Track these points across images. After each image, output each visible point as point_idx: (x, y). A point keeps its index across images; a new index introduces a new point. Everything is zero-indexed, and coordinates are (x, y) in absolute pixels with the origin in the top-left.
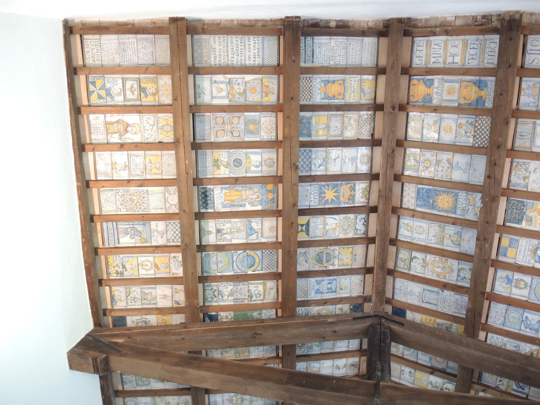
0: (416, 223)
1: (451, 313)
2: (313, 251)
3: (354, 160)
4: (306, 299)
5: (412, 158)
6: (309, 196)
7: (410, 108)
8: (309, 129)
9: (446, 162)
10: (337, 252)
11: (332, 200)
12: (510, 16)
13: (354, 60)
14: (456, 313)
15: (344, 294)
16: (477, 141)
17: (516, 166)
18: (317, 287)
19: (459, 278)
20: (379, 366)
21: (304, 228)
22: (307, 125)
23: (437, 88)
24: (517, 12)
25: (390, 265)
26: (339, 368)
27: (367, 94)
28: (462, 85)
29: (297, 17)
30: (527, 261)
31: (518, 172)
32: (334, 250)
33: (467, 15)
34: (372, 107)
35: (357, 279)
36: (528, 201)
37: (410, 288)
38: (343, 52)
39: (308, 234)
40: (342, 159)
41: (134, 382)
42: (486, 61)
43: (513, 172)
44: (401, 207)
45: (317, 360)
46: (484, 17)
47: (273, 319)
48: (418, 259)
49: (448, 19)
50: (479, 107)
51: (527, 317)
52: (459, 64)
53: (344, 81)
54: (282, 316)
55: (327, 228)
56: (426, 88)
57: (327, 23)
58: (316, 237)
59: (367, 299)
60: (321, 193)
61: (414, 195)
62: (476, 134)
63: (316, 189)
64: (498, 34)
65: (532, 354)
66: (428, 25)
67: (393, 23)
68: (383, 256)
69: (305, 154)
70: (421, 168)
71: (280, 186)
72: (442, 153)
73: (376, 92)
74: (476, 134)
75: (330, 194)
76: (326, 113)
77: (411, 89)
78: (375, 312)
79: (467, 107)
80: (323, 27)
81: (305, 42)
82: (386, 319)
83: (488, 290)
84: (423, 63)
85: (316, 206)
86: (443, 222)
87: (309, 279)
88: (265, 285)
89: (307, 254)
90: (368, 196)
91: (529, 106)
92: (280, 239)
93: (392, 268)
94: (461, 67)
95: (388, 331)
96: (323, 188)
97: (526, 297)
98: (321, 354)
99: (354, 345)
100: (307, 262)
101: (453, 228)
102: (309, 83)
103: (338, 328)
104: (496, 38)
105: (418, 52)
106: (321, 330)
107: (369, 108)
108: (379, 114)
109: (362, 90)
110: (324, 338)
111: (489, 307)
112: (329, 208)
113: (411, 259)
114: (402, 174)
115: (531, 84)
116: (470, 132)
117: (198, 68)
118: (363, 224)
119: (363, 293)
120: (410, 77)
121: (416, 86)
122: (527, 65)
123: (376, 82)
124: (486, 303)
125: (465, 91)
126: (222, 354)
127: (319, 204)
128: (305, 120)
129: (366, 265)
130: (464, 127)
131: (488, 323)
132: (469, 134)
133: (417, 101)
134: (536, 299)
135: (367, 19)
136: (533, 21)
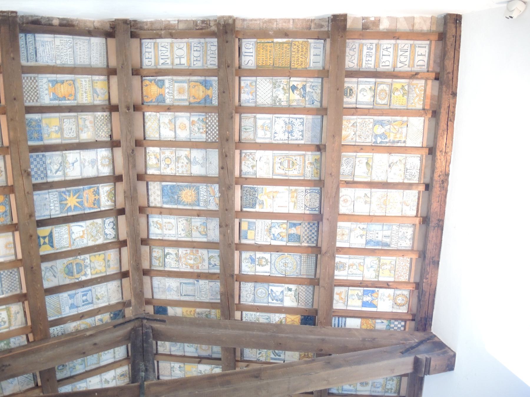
0: (165, 220)
1: (208, 301)
2: (60, 264)
3: (94, 162)
4: (60, 317)
5: (153, 157)
6: (48, 204)
7: (145, 109)
8: (40, 132)
9: (185, 158)
10: (88, 261)
11: (75, 206)
12: (225, 21)
13: (82, 60)
14: (212, 299)
15: (102, 304)
16: (209, 136)
17: (244, 156)
18: (70, 302)
19: (210, 266)
20: (142, 366)
21: (47, 240)
22: (37, 128)
23: (168, 88)
24: (230, 17)
25: (146, 265)
27: (100, 94)
28: (190, 84)
29: (13, 12)
30: (265, 240)
31: (247, 162)
32: (84, 260)
33: (188, 19)
34: (107, 108)
35: (113, 285)
36: (258, 186)
37: (167, 285)
38: (69, 52)
39: (52, 246)
40: (81, 163)
42: (209, 63)
43: (243, 162)
44: (149, 206)
45: (82, 379)
46: (203, 22)
47: (24, 346)
48: (171, 254)
49: (171, 22)
50: (207, 105)
51: (272, 290)
52: (186, 65)
53: (74, 81)
54: (34, 341)
55: (74, 236)
56: (159, 89)
57: (49, 20)
58: (61, 248)
59: (126, 304)
60: (62, 201)
61: (159, 193)
62: (207, 130)
63: (56, 196)
64: (216, 37)
65: (281, 322)
66: (154, 27)
67: (119, 24)
68: (136, 257)
69: (38, 159)
70: (163, 166)
71: (12, 196)
72: (180, 150)
73: (109, 93)
74: (207, 130)
75: (72, 201)
76: (57, 115)
77: (144, 90)
78: (136, 315)
79: (197, 105)
80: (45, 25)
81: (26, 39)
82: (148, 319)
83: (236, 272)
84: (153, 65)
85: (58, 214)
86: (189, 216)
87: (61, 295)
88: (8, 310)
89: (54, 267)
90: (114, 199)
91: (249, 102)
92: (20, 256)
93: (148, 268)
94: (187, 68)
95: (150, 331)
96: (63, 194)
97: (269, 272)
98: (87, 372)
100: (55, 277)
101: (200, 220)
102: (35, 83)
103: (97, 340)
104: (215, 41)
105: (147, 53)
106: (80, 345)
107: (103, 109)
108: (115, 114)
109: (94, 91)
110: (84, 353)
111: (240, 287)
112: (73, 216)
113: (165, 256)
114: (146, 173)
115: (249, 82)
116: (203, 129)
118: (113, 228)
119: (123, 298)
120: (142, 78)
121: (149, 86)
122: (243, 66)
123: (109, 83)
124: (237, 284)
125: (193, 91)
127: (61, 212)
128: (34, 123)
129: (121, 269)
130: (196, 125)
131: (241, 303)
132: (201, 130)
133: (151, 101)
134: (276, 273)
135: (92, 19)
136: (245, 26)
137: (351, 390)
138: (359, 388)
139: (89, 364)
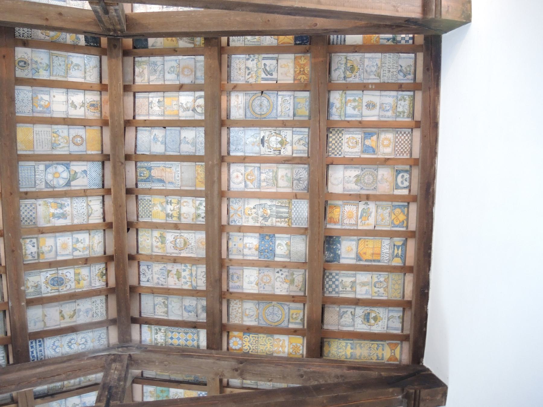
26: (75, 107)
99: (92, 77)
137: (356, 116)
138: (365, 112)
139: (54, 74)
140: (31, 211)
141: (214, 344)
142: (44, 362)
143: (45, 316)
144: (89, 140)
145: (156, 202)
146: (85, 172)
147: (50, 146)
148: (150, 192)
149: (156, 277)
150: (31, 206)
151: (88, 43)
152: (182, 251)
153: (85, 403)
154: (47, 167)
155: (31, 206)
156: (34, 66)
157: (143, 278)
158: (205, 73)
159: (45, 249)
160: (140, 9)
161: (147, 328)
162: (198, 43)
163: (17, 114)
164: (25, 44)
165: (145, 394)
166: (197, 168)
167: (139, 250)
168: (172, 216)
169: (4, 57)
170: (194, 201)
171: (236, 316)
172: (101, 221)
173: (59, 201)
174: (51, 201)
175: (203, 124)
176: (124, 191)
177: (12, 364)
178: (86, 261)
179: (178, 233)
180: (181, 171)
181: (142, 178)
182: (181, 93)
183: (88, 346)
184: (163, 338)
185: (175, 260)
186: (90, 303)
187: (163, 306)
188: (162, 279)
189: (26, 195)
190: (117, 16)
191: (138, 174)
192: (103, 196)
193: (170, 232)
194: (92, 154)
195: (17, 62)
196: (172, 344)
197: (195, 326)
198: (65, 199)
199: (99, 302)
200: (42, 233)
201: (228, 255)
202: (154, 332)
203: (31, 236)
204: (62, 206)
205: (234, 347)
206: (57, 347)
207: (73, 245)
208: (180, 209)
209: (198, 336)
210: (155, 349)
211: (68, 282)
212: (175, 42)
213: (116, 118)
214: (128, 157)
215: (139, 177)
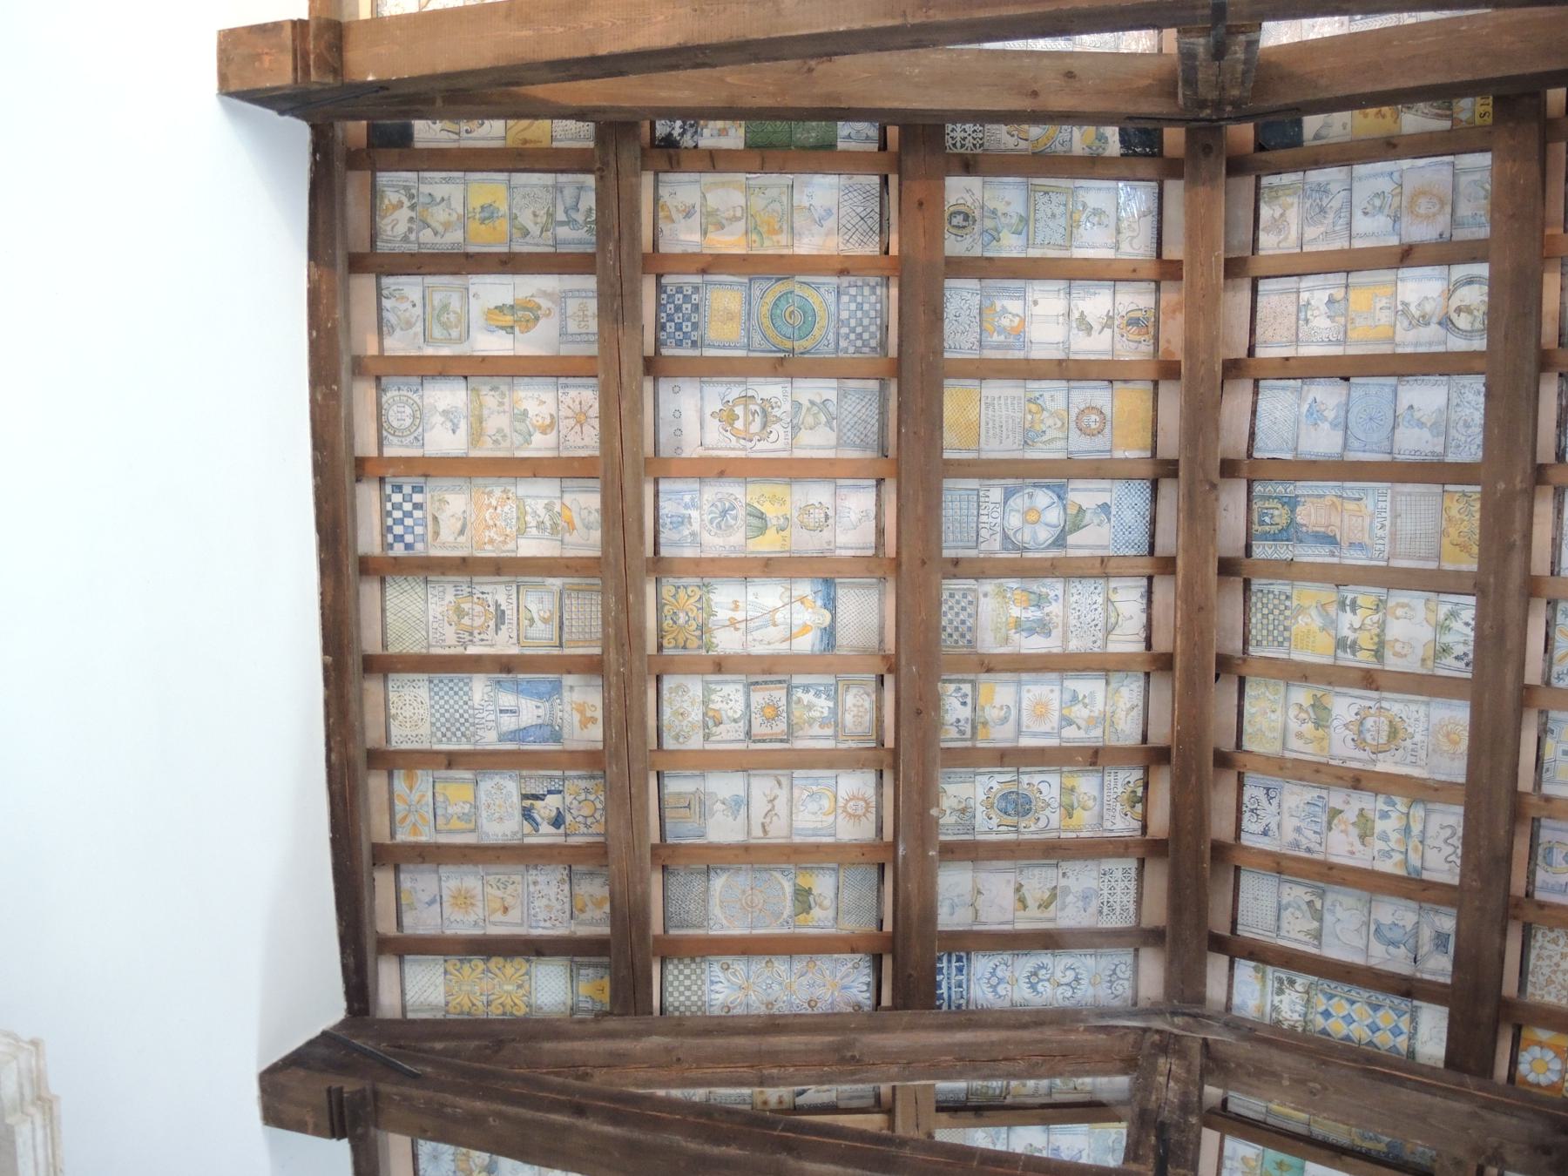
26: (1089, 329)
41: (419, 328)
99: (1136, 243)
117: (670, 560)
126: (704, 233)
139: (1038, 241)
140: (964, 609)
141: (1470, 1050)
142: (975, 1017)
143: (979, 892)
144: (1119, 420)
145: (1306, 603)
146: (1105, 508)
147: (1019, 437)
148: (1287, 570)
149: (1290, 824)
150: (965, 596)
151: (1128, 148)
152: (1381, 756)
153: (1057, 1149)
154: (1008, 494)
155: (965, 596)
156: (989, 223)
157: (1249, 823)
158: (1495, 207)
159: (992, 713)
160: (1278, 34)
161: (1251, 971)
162: (1464, 116)
163: (947, 355)
164: (968, 165)
165: (1228, 1163)
166: (1447, 503)
167: (1245, 738)
168: (1354, 647)
169: (921, 204)
170: (1432, 605)
171: (1550, 982)
172: (1139, 647)
173: (1034, 586)
174: (1015, 586)
175: (1479, 364)
176: (1213, 568)
177: (887, 1009)
178: (1095, 758)
179: (1370, 699)
180: (1393, 509)
181: (1267, 528)
182: (1405, 272)
183: (1079, 994)
184: (1298, 1008)
185: (1357, 781)
186: (1095, 874)
187: (1308, 914)
188: (1310, 834)
189: (956, 567)
190: (1246, 62)
191: (1256, 518)
192: (1150, 579)
193: (1345, 695)
194: (1126, 459)
195: (946, 216)
196: (1324, 1032)
197: (1409, 989)
198: (1048, 581)
199: (1118, 874)
200: (989, 671)
201: (1538, 783)
202: (1271, 985)
203: (959, 676)
204: (1040, 601)
205: (1531, 1078)
206: (1000, 981)
207: (1061, 709)
208: (1382, 626)
209: (1414, 1020)
210: (1273, 1036)
211: (1043, 809)
212: (1389, 120)
213: (1203, 356)
214: (1229, 468)
215: (1256, 527)
